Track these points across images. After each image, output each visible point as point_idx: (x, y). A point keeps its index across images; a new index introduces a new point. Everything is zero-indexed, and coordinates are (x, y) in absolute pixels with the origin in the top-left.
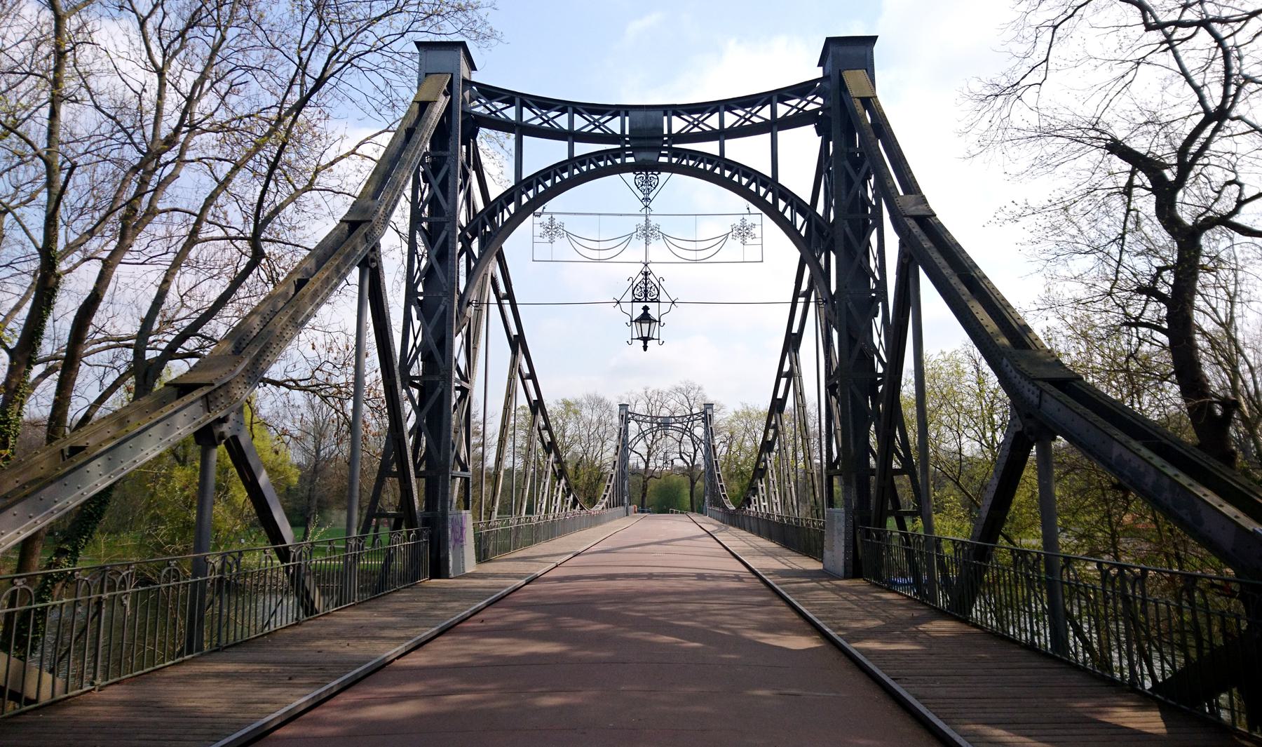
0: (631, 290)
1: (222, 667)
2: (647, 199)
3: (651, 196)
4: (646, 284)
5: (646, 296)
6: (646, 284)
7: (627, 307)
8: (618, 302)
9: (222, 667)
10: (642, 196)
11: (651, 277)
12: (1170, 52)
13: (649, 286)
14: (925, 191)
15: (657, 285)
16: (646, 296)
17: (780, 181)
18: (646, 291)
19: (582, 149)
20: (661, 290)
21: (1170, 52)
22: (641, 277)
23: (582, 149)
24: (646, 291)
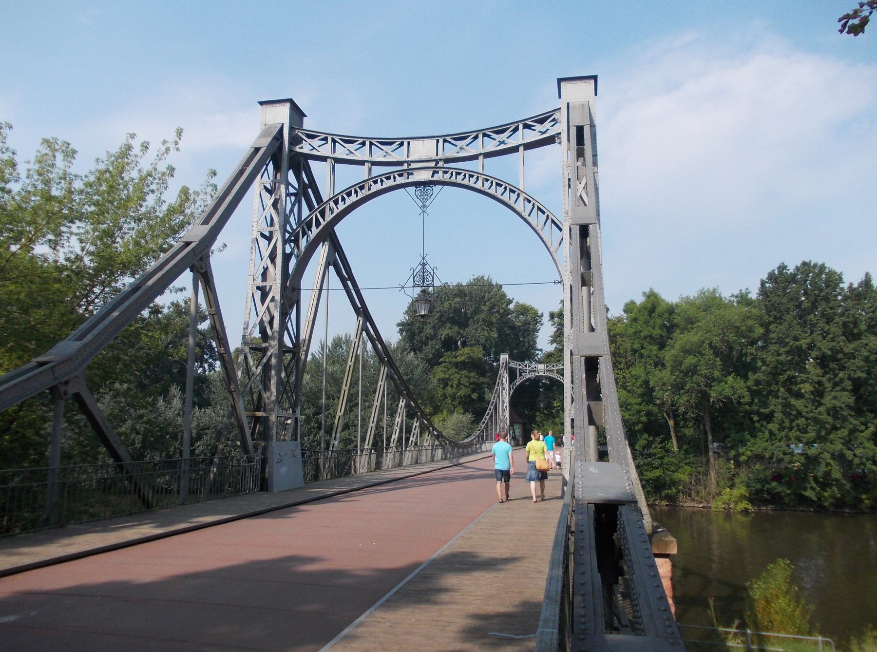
0: (412, 277)
1: (386, 488)
2: (424, 206)
3: (427, 204)
4: (423, 273)
5: (423, 282)
6: (423, 273)
7: (409, 291)
8: (403, 287)
9: (386, 488)
10: (421, 204)
11: (427, 267)
12: (412, 142)
13: (425, 274)
14: (599, 192)
15: (432, 274)
16: (423, 282)
17: (335, 228)
18: (423, 278)
19: (377, 171)
20: (435, 277)
21: (412, 142)
22: (420, 267)
23: (377, 171)
24: (423, 278)
